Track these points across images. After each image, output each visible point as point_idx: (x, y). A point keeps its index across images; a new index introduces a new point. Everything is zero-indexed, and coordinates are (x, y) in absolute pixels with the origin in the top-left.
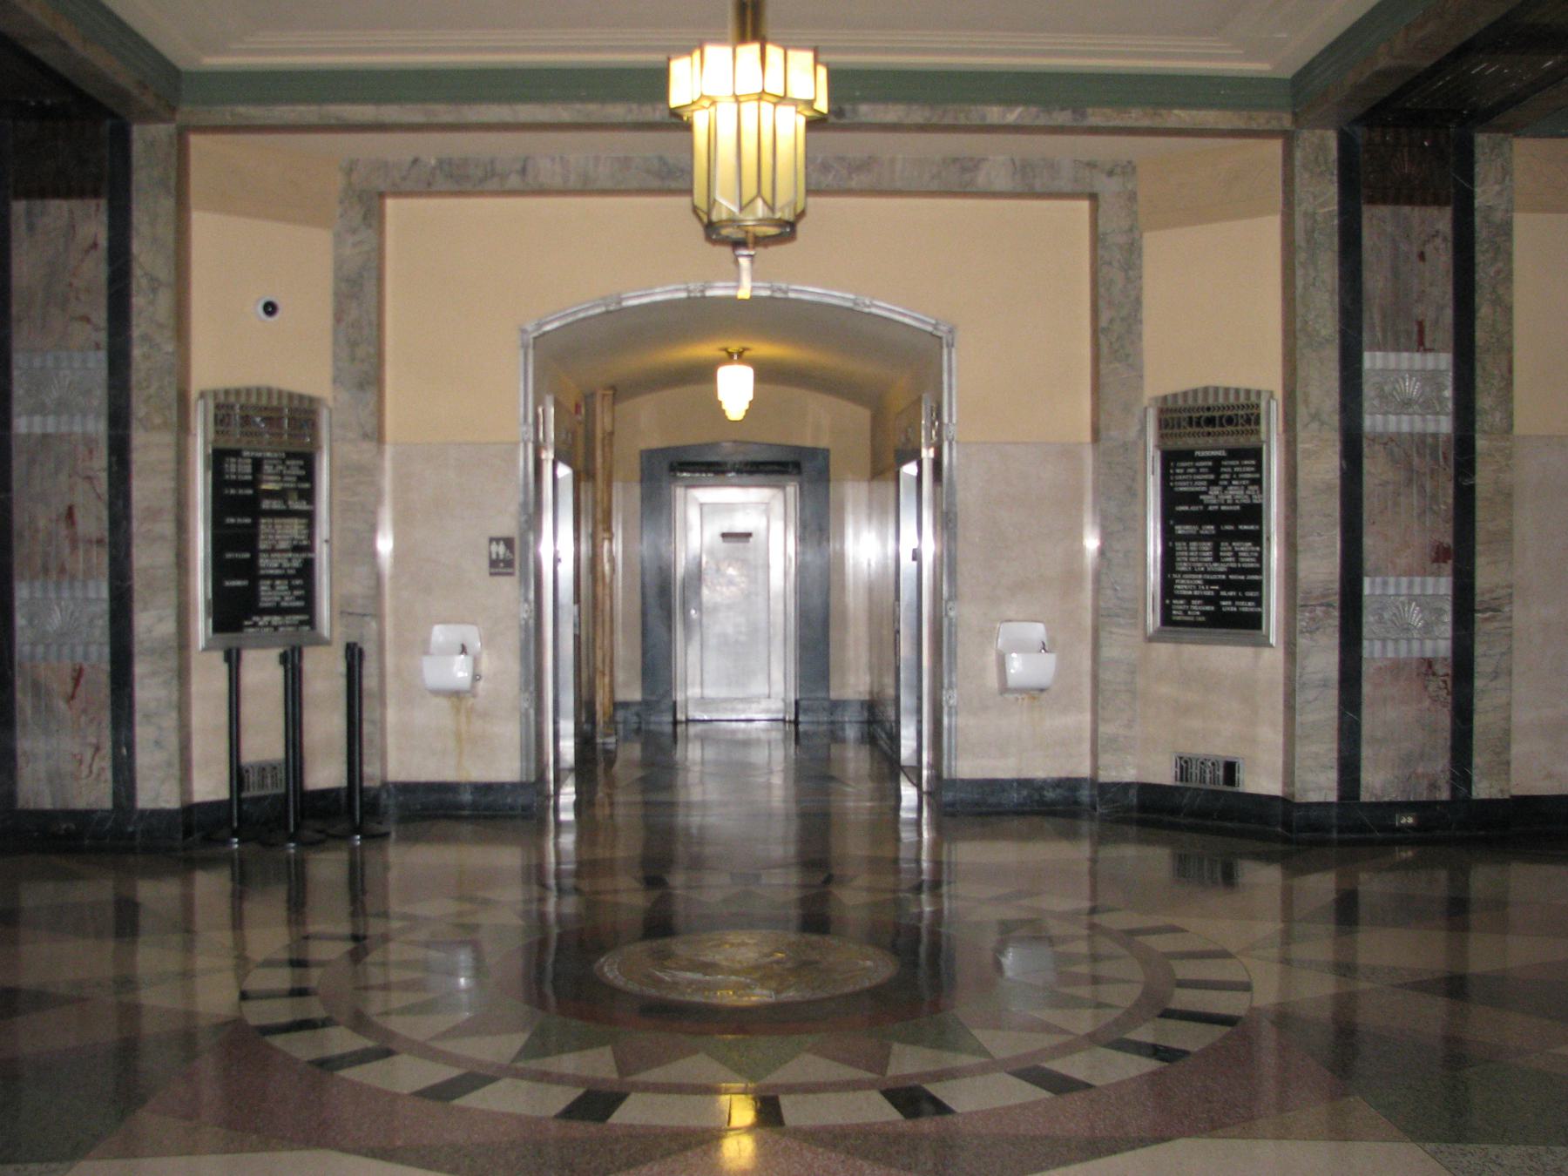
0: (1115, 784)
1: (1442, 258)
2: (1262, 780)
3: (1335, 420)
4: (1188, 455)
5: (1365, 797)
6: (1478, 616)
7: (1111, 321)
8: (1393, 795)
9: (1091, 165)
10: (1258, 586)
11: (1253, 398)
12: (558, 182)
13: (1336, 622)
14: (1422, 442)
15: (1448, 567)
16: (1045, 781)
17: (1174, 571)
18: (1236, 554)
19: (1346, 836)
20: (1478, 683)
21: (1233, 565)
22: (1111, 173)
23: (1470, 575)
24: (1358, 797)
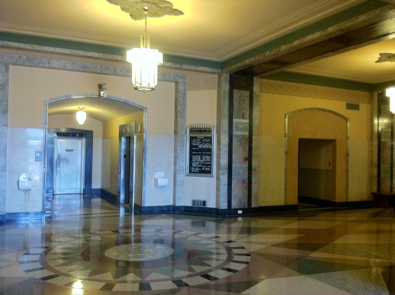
0: (179, 206)
1: (247, 101)
2: (211, 204)
3: (228, 132)
4: (196, 138)
5: (233, 208)
6: (253, 171)
7: (180, 109)
8: (237, 207)
9: (177, 76)
10: (210, 165)
11: (210, 126)
12: (57, 66)
13: (227, 172)
14: (243, 136)
15: (247, 162)
16: (163, 206)
17: (192, 161)
18: (206, 158)
19: (229, 216)
20: (253, 184)
21: (205, 161)
22: (181, 78)
23: (251, 163)
24: (231, 208)
